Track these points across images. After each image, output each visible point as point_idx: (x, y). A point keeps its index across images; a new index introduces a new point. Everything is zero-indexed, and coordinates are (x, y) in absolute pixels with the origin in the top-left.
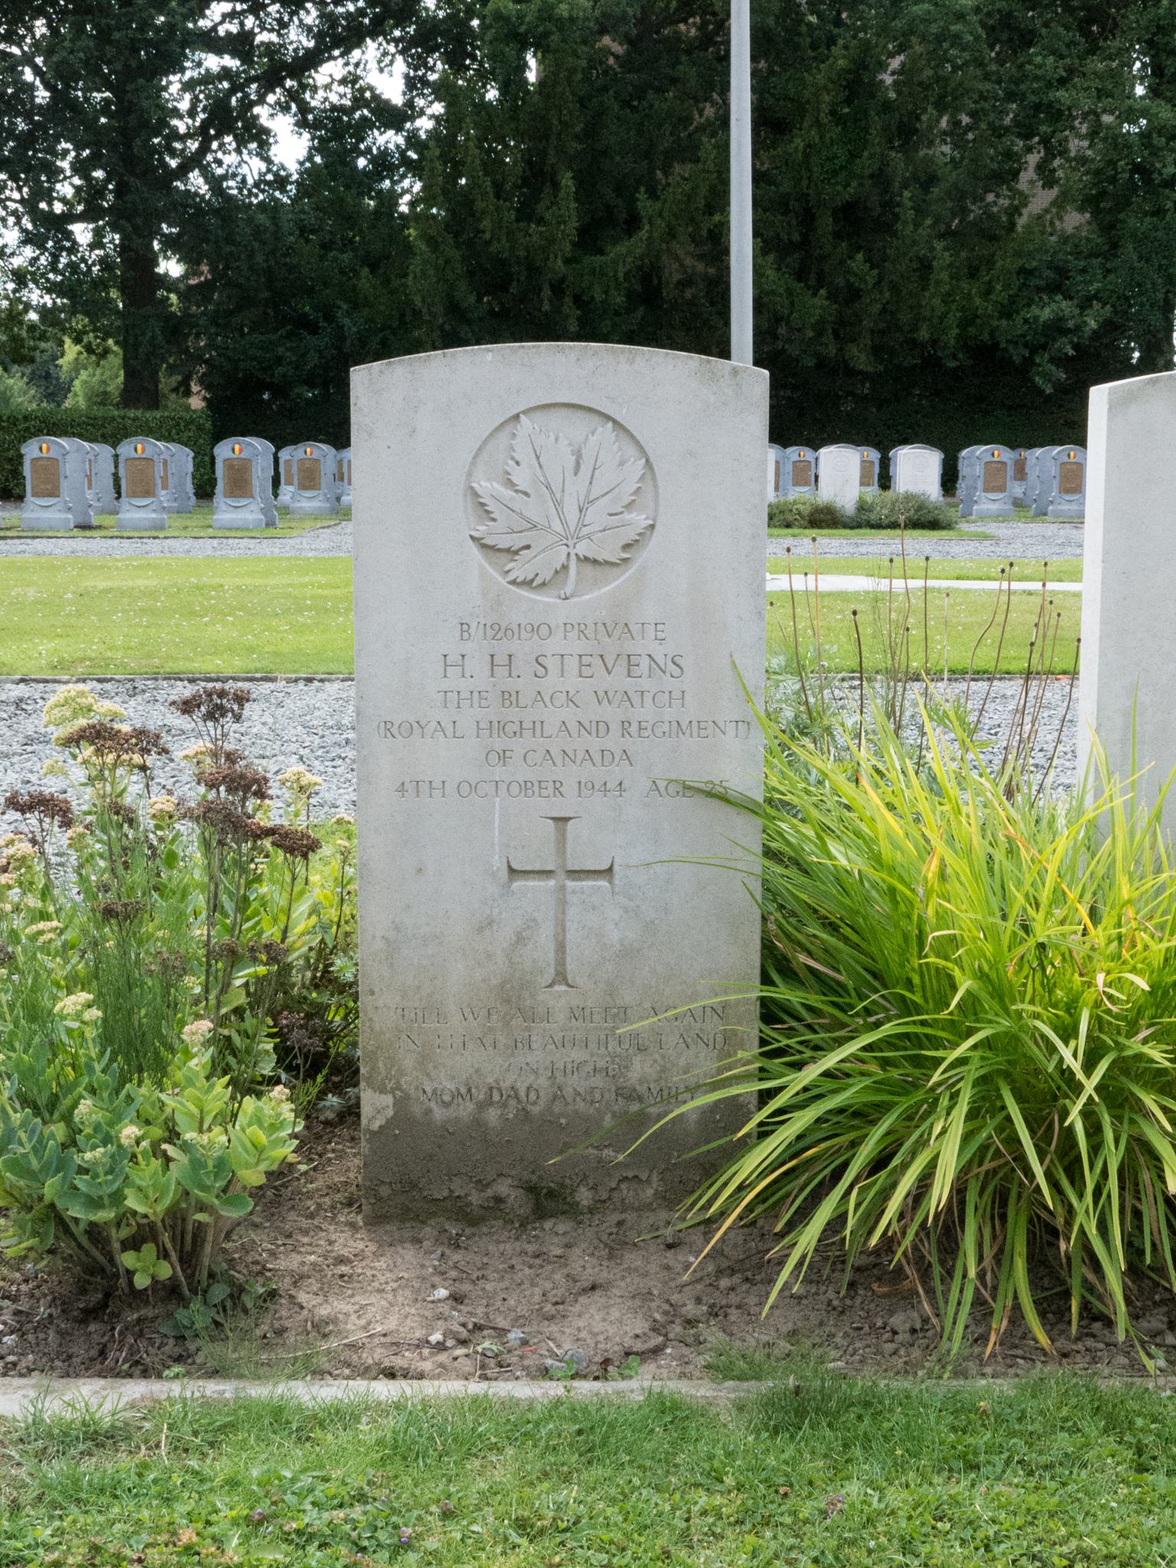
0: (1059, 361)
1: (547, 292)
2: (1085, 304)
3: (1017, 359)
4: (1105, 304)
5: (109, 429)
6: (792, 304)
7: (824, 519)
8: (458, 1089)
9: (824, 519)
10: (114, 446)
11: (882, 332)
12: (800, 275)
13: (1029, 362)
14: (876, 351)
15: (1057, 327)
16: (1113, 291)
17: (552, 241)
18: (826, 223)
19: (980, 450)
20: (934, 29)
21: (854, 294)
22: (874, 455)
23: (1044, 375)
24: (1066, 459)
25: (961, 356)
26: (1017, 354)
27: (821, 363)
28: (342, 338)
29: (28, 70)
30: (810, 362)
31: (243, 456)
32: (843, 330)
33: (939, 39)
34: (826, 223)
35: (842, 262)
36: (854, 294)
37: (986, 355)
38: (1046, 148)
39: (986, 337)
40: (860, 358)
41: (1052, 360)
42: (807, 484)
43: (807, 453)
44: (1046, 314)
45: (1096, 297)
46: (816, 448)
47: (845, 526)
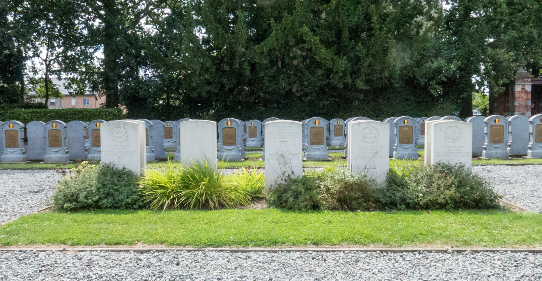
3: (423, 84)
4: (458, 61)
5: (80, 116)
6: (334, 64)
10: (329, 120)
11: (369, 74)
12: (338, 53)
13: (427, 85)
14: (367, 82)
15: (438, 71)
16: (461, 56)
21: (358, 59)
24: (494, 124)
25: (400, 82)
26: (423, 81)
30: (341, 86)
31: (14, 129)
32: (355, 73)
34: (346, 34)
35: (353, 48)
36: (358, 59)
37: (411, 82)
38: (429, 6)
39: (410, 75)
40: (361, 84)
41: (436, 83)
42: (341, 135)
43: (340, 121)
44: (435, 65)
45: (453, 58)
46: (262, 119)
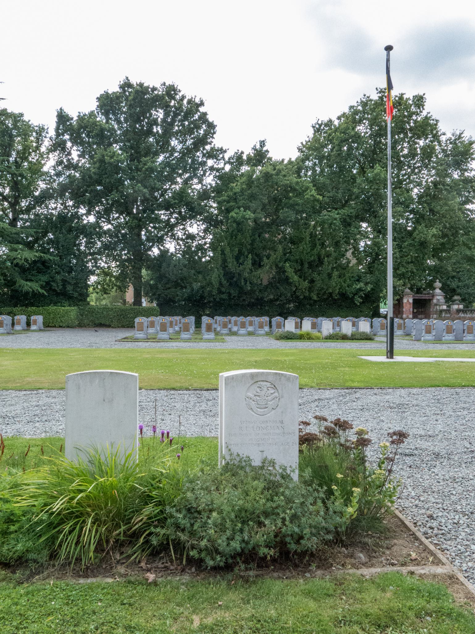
0: (361, 297)
1: (243, 281)
2: (366, 284)
3: (351, 297)
7: (344, 338)
8: (342, 547)
9: (344, 338)
13: (353, 297)
15: (360, 290)
17: (245, 269)
18: (306, 265)
19: (275, 319)
20: (330, 222)
22: (299, 320)
23: (357, 301)
26: (351, 296)
27: (305, 297)
28: (193, 290)
29: (419, 165)
30: (302, 297)
32: (310, 289)
33: (331, 224)
37: (343, 296)
44: (358, 287)
47: (350, 339)
